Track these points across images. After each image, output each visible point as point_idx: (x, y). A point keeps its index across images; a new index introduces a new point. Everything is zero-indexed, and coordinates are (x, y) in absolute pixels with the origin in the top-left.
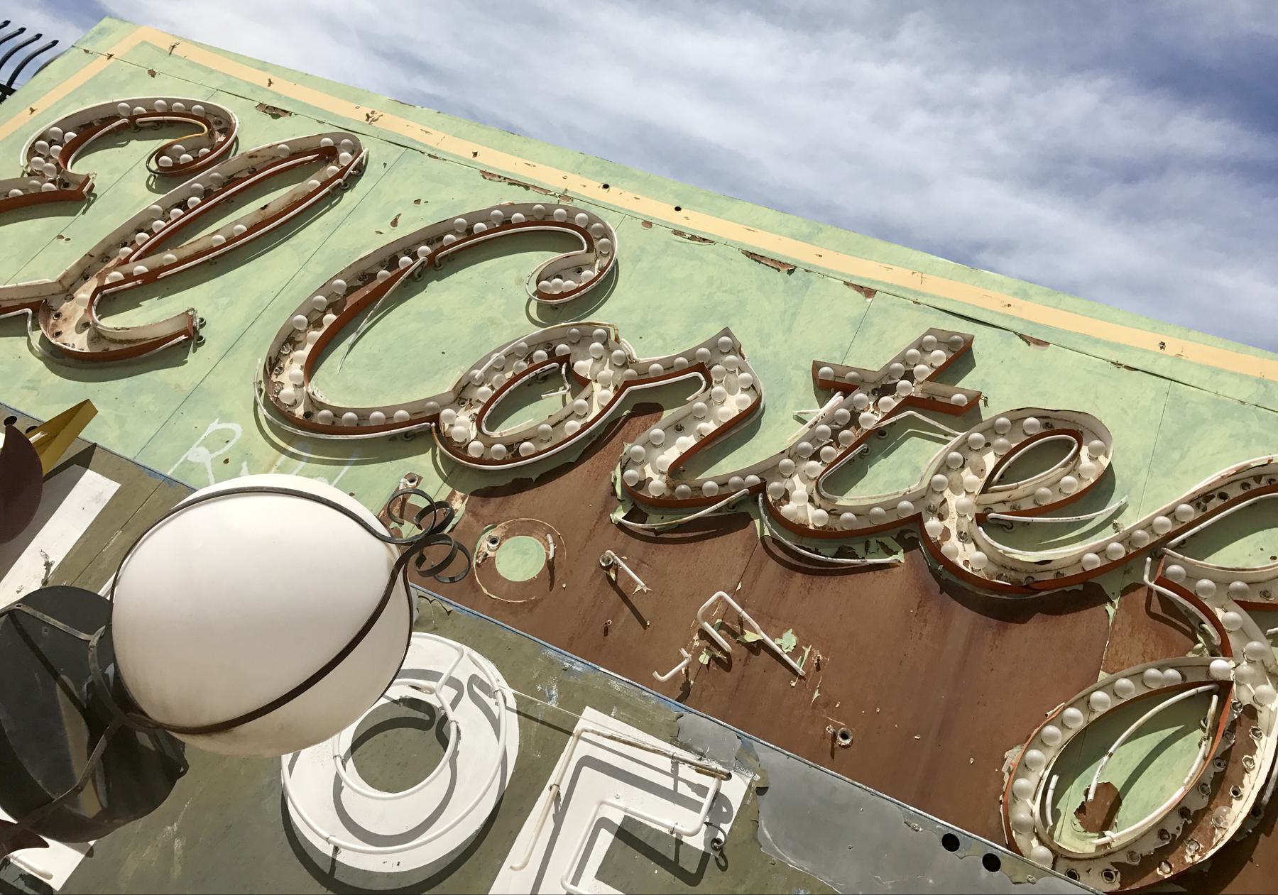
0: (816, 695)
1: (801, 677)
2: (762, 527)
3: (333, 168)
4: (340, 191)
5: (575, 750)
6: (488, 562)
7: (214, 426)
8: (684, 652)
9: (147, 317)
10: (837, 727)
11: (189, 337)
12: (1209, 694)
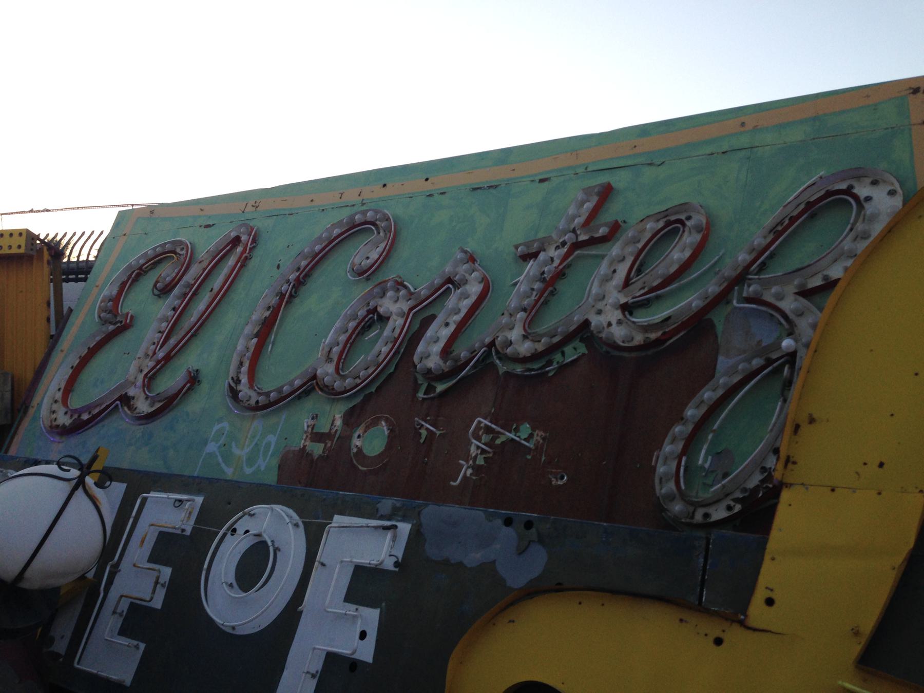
0: (543, 458)
3: (239, 249)
4: (244, 262)
6: (360, 450)
7: (217, 427)
8: (461, 462)
9: (169, 382)
12: (782, 366)
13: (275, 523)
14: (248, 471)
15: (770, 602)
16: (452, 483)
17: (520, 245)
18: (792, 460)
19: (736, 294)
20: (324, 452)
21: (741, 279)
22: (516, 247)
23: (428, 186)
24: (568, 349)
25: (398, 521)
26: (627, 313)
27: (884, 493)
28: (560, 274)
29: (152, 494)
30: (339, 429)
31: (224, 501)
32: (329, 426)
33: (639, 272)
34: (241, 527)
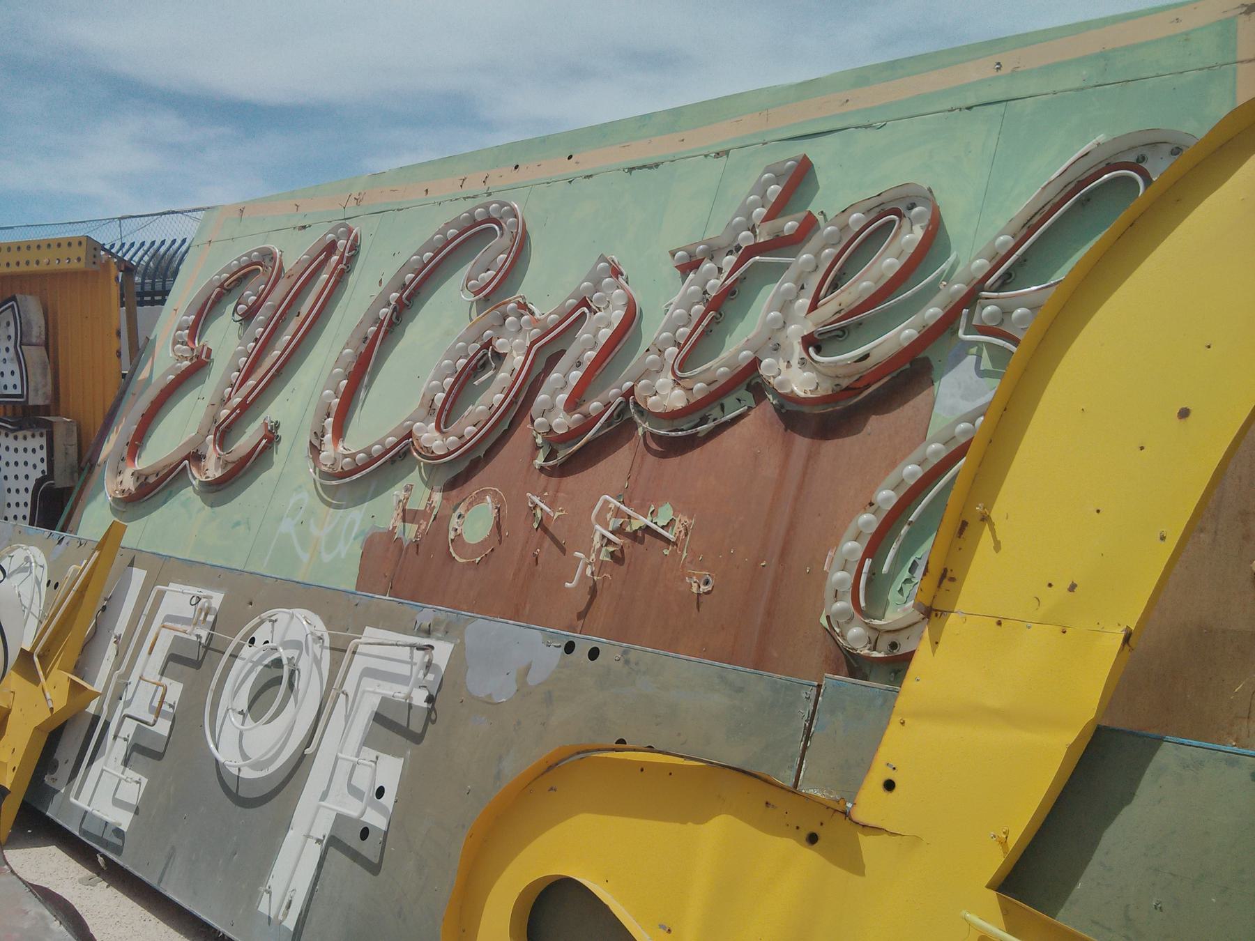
1: (675, 544)
2: (643, 427)
3: (335, 258)
4: (341, 277)
5: (359, 663)
8: (577, 554)
10: (699, 577)
11: (271, 437)
13: (294, 627)
14: (327, 558)
15: (889, 785)
16: (568, 584)
17: (679, 250)
18: (949, 575)
19: (963, 321)
20: (416, 536)
21: (971, 299)
22: (673, 254)
23: (571, 168)
24: (729, 401)
25: (438, 639)
26: (811, 350)
27: (1068, 630)
28: (729, 293)
29: (172, 586)
30: (437, 506)
31: (252, 595)
32: (425, 501)
33: (835, 286)
34: (260, 635)
